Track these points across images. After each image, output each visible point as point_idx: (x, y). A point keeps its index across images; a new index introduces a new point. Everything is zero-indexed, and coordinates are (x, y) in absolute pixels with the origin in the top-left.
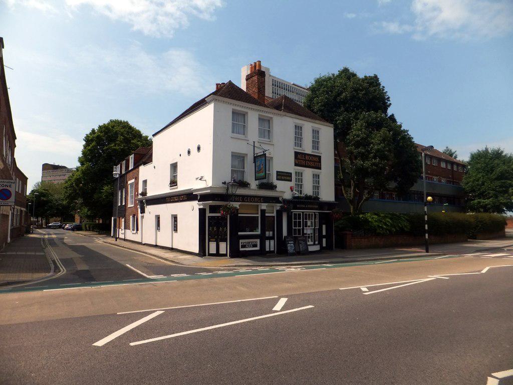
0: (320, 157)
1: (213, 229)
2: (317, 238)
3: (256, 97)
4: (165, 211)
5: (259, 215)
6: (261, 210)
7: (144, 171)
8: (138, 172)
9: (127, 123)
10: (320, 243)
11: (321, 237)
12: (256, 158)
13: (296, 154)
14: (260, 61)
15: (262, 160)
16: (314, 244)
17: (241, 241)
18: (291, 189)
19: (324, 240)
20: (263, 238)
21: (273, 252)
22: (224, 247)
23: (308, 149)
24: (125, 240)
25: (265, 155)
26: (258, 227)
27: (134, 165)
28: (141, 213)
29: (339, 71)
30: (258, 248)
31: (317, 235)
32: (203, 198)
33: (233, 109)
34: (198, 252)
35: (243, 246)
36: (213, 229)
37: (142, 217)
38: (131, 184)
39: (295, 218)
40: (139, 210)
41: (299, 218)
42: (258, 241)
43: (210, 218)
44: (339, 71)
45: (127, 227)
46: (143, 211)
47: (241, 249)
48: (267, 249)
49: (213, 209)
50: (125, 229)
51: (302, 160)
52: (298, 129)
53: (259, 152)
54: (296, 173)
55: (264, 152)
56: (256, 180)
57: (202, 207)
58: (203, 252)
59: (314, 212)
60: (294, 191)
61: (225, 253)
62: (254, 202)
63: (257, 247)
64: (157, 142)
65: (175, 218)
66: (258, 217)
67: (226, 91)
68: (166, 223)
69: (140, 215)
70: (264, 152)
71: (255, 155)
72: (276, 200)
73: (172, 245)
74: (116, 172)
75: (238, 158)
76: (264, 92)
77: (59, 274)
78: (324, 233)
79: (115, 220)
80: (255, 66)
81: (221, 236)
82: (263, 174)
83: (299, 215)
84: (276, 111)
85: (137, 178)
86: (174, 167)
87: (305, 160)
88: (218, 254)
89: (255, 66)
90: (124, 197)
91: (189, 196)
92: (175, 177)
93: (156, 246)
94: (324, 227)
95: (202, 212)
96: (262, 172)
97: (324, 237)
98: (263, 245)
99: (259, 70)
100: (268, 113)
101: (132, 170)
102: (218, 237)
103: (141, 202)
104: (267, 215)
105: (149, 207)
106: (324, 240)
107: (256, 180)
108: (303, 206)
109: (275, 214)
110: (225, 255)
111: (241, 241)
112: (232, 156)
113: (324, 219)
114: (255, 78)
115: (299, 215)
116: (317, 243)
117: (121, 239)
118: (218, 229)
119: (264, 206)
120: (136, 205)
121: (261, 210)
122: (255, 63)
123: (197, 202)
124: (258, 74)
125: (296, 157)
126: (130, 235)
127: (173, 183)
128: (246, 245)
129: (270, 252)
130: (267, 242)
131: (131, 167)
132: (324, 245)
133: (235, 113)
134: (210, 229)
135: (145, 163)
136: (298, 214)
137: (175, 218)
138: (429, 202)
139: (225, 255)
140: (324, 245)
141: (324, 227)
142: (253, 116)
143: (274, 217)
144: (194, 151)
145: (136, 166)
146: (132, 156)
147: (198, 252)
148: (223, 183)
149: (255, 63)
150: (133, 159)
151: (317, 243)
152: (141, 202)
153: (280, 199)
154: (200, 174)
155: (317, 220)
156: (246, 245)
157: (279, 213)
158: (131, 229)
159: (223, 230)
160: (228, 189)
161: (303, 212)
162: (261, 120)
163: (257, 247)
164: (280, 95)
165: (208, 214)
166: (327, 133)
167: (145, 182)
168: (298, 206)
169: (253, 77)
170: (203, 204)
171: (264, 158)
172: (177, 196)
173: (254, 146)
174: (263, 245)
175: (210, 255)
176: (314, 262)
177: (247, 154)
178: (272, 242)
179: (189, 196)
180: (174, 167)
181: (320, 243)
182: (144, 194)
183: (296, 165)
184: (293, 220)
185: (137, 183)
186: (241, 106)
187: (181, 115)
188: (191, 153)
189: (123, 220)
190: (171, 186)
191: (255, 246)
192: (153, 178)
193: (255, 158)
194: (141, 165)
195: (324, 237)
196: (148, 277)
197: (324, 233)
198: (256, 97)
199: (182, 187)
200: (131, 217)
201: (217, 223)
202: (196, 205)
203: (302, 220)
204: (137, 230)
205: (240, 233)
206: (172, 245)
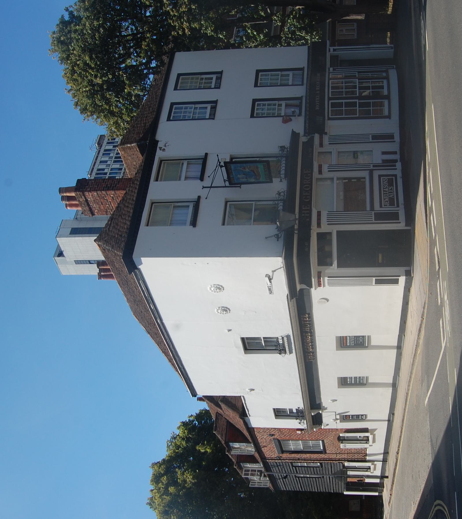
4: (330, 363)
7: (260, 418)
12: (232, 182)
14: (60, 188)
16: (387, 78)
29: (61, 63)
41: (340, 105)
44: (61, 63)
50: (365, 461)
55: (221, 167)
56: (271, 182)
59: (329, 79)
66: (338, 232)
68: (353, 363)
71: (227, 184)
74: (259, 481)
75: (236, 213)
76: (101, 228)
79: (351, 486)
82: (261, 167)
83: (333, 105)
86: (250, 345)
89: (69, 198)
93: (399, 348)
94: (347, 181)
96: (257, 168)
99: (76, 189)
107: (271, 182)
114: (90, 196)
116: (384, 74)
122: (63, 198)
123: (313, 290)
126: (375, 448)
131: (249, 449)
135: (243, 414)
136: (333, 88)
138: (242, 499)
144: (223, 299)
149: (63, 198)
158: (366, 446)
161: (329, 99)
167: (279, 413)
168: (317, 108)
169: (87, 200)
171: (233, 166)
173: (211, 187)
180: (250, 345)
182: (299, 415)
187: (159, 343)
192: (268, 393)
194: (246, 424)
200: (342, 446)
203: (344, 101)
204: (366, 430)
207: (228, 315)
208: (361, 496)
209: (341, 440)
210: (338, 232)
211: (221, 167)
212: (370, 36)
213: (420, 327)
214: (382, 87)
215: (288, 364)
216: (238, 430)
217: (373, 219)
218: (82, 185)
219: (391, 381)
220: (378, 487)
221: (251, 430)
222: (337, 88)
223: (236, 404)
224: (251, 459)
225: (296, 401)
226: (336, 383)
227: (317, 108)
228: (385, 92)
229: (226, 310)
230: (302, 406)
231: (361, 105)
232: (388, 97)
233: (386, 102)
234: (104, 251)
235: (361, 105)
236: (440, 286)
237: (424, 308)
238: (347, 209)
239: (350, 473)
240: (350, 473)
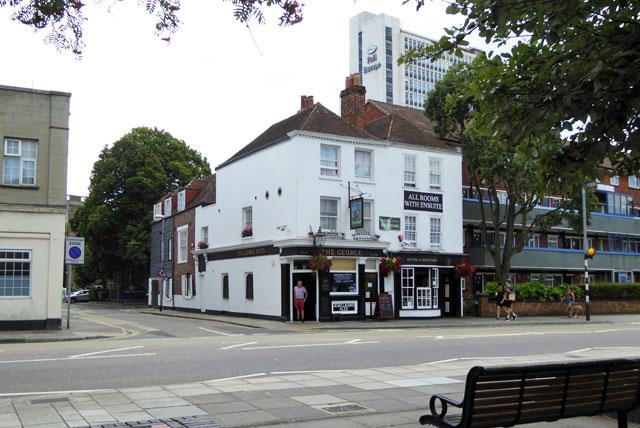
0: (440, 196)
4: (237, 268)
5: (357, 271)
6: (360, 266)
13: (407, 194)
15: (359, 207)
17: (333, 303)
18: (400, 239)
19: (447, 304)
20: (361, 299)
23: (423, 186)
25: (362, 199)
26: (298, 269)
27: (187, 205)
28: (200, 271)
30: (355, 312)
32: (288, 251)
33: (322, 145)
35: (336, 309)
38: (183, 233)
39: (405, 275)
42: (356, 303)
46: (202, 268)
51: (414, 200)
52: (411, 160)
53: (355, 195)
54: (406, 217)
56: (352, 228)
57: (285, 262)
60: (404, 241)
64: (224, 182)
65: (250, 278)
68: (238, 286)
69: (197, 274)
72: (378, 252)
78: (447, 295)
79: (156, 285)
82: (359, 222)
85: (192, 224)
87: (420, 201)
91: (268, 250)
92: (250, 223)
94: (447, 287)
95: (285, 268)
97: (447, 299)
98: (361, 308)
103: (201, 257)
105: (211, 263)
106: (447, 304)
107: (352, 228)
108: (416, 260)
109: (377, 270)
111: (333, 303)
112: (322, 200)
116: (435, 307)
117: (166, 308)
119: (362, 260)
121: (360, 266)
124: (353, 90)
125: (406, 198)
127: (247, 233)
130: (368, 305)
131: (182, 206)
132: (448, 310)
135: (204, 205)
137: (250, 278)
141: (447, 287)
142: (348, 149)
143: (376, 274)
145: (191, 206)
152: (201, 257)
153: (385, 251)
160: (315, 242)
165: (293, 271)
166: (451, 165)
167: (205, 229)
168: (409, 259)
174: (361, 308)
177: (339, 198)
180: (248, 211)
181: (441, 307)
182: (203, 246)
183: (406, 208)
184: (413, 278)
188: (270, 194)
191: (352, 309)
192: (217, 225)
193: (350, 201)
195: (447, 299)
197: (447, 295)
199: (259, 238)
202: (277, 261)
204: (194, 293)
205: (331, 294)
207: (265, 198)
208: (147, 291)
215: (236, 241)
217: (426, 288)
219: (176, 306)
220: (155, 305)
223: (210, 200)
225: (214, 245)
226: (249, 271)
227: (409, 259)
230: (210, 247)
231: (410, 290)
232: (415, 308)
235: (410, 290)
236: (508, 385)
238: (27, 294)
239: (165, 282)
240: (165, 282)
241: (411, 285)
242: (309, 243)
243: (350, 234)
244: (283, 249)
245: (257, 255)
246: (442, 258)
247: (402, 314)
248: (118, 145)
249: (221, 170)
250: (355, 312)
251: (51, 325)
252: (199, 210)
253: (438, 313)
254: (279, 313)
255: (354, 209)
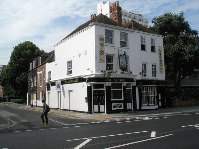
1: (96, 98)
2: (156, 102)
3: (117, 21)
5: (122, 89)
8: (45, 67)
9: (16, 48)
10: (158, 104)
11: (158, 101)
16: (155, 105)
17: (113, 104)
19: (160, 102)
21: (131, 110)
22: (103, 108)
24: (37, 106)
27: (36, 66)
28: (48, 90)
30: (123, 108)
31: (156, 99)
32: (90, 80)
33: (105, 29)
34: (87, 111)
36: (96, 98)
37: (49, 93)
38: (41, 75)
40: (46, 89)
42: (122, 104)
43: (94, 92)
45: (38, 99)
47: (113, 109)
48: (128, 108)
49: (96, 86)
56: (120, 69)
57: (89, 85)
58: (90, 110)
59: (154, 87)
61: (104, 111)
62: (119, 82)
63: (122, 107)
66: (122, 90)
67: (99, 20)
69: (47, 91)
70: (124, 53)
72: (131, 80)
73: (69, 108)
77: (12, 125)
78: (160, 98)
80: (115, 4)
81: (101, 102)
83: (146, 88)
84: (128, 29)
86: (69, 63)
88: (99, 112)
89: (115, 4)
90: (35, 81)
91: (81, 80)
94: (160, 95)
95: (89, 89)
97: (160, 100)
98: (125, 106)
99: (118, 6)
100: (126, 30)
101: (35, 69)
102: (99, 102)
104: (127, 89)
106: (160, 102)
107: (120, 69)
109: (131, 88)
110: (104, 112)
111: (113, 104)
113: (160, 90)
114: (116, 11)
115: (146, 88)
116: (156, 104)
118: (99, 97)
120: (44, 87)
122: (115, 2)
124: (116, 9)
128: (116, 106)
129: (130, 110)
131: (40, 64)
132: (160, 105)
133: (107, 31)
134: (93, 98)
139: (104, 112)
140: (160, 105)
141: (160, 95)
143: (131, 90)
146: (35, 61)
147: (87, 111)
148: (101, 71)
149: (115, 2)
150: (41, 60)
151: (156, 104)
153: (135, 80)
154: (88, 65)
155: (156, 91)
156: (116, 106)
157: (134, 88)
159: (102, 98)
161: (148, 87)
162: (121, 34)
163: (122, 107)
164: (127, 21)
165: (93, 89)
167: (50, 72)
170: (90, 84)
172: (72, 80)
173: (118, 50)
174: (125, 106)
175: (95, 112)
176: (152, 115)
177: (114, 55)
178: (130, 104)
179: (81, 80)
180: (69, 63)
181: (158, 104)
184: (142, 91)
185: (44, 73)
186: (110, 28)
188: (78, 56)
189: (35, 95)
190: (67, 74)
191: (121, 107)
192: (55, 71)
193: (119, 56)
194: (47, 63)
195: (160, 100)
196: (65, 125)
197: (160, 98)
198: (117, 21)
199: (75, 75)
201: (99, 95)
202: (85, 85)
203: (147, 91)
205: (112, 100)
206: (69, 108)
209: (43, 92)
210: (122, 90)
211: (124, 53)
212: (2, 90)
213: (74, 117)
214: (152, 103)
215: (65, 76)
216: (44, 61)
218: (119, 9)
219: (37, 105)
221: (45, 63)
222: (151, 89)
224: (37, 64)
228: (150, 105)
229: (80, 55)
232: (148, 105)
233: (154, 104)
234: (98, 16)
237: (73, 116)
241: (146, 95)
242: (102, 76)
243: (119, 71)
244: (88, 79)
245: (75, 83)
246: (158, 82)
247: (143, 108)
248: (11, 59)
249: (56, 47)
250: (123, 108)
251: (55, 46)
252: (47, 65)
253: (156, 107)
254: (86, 110)
255: (121, 60)
